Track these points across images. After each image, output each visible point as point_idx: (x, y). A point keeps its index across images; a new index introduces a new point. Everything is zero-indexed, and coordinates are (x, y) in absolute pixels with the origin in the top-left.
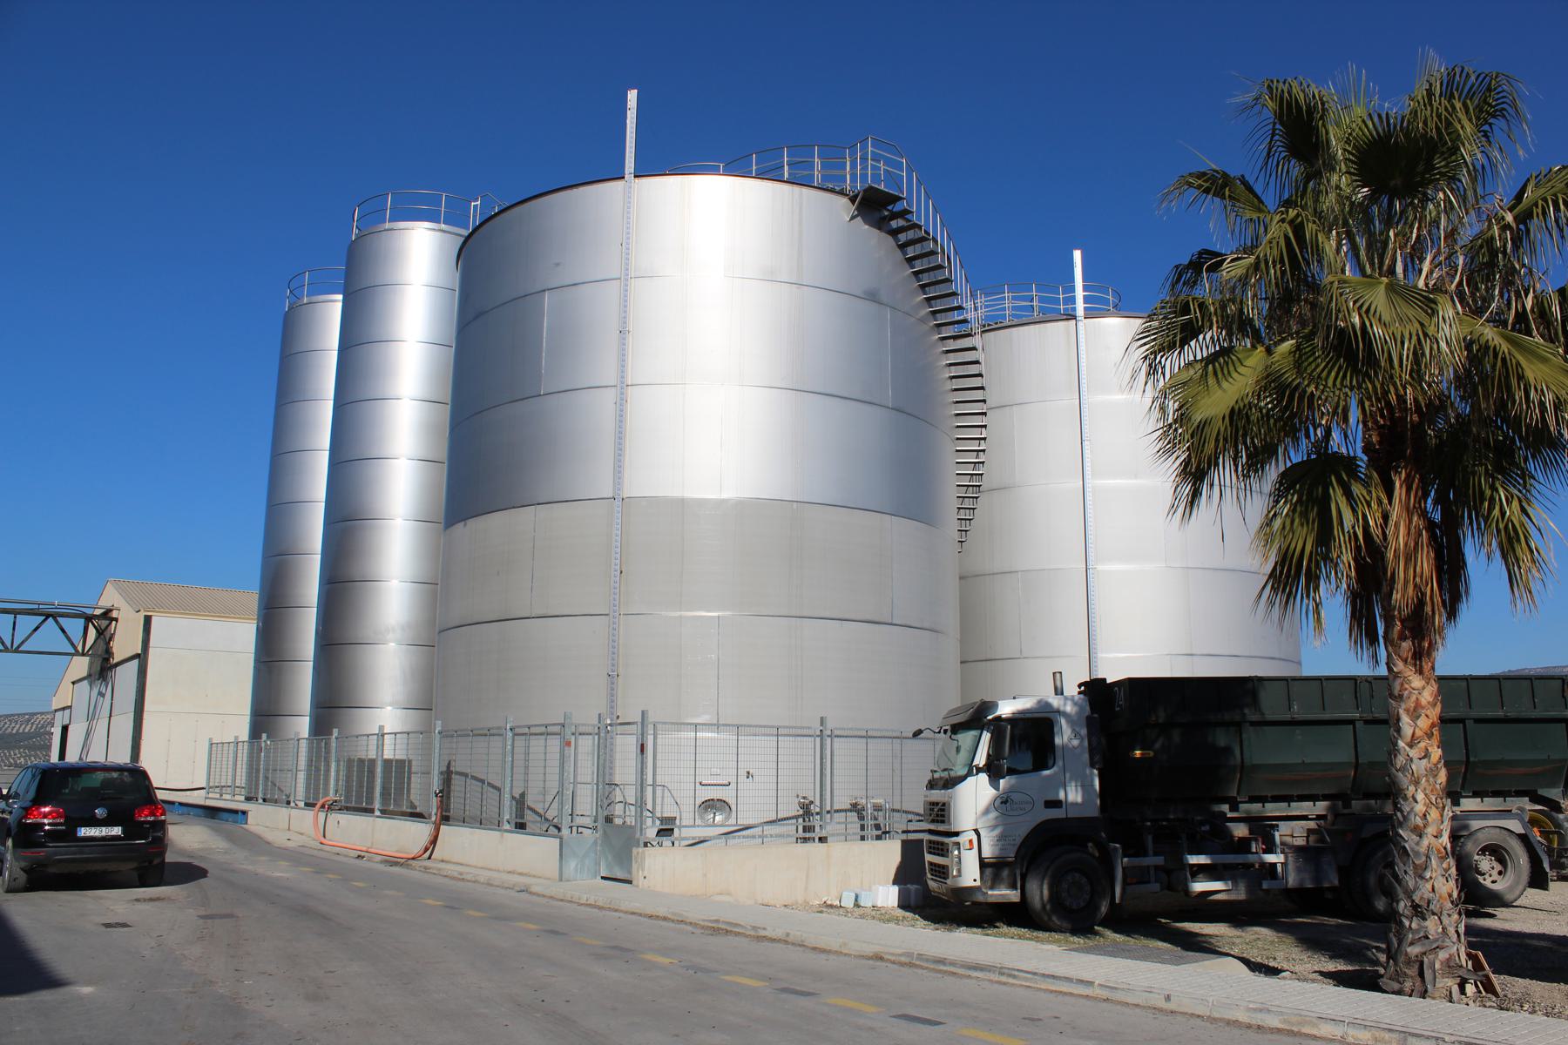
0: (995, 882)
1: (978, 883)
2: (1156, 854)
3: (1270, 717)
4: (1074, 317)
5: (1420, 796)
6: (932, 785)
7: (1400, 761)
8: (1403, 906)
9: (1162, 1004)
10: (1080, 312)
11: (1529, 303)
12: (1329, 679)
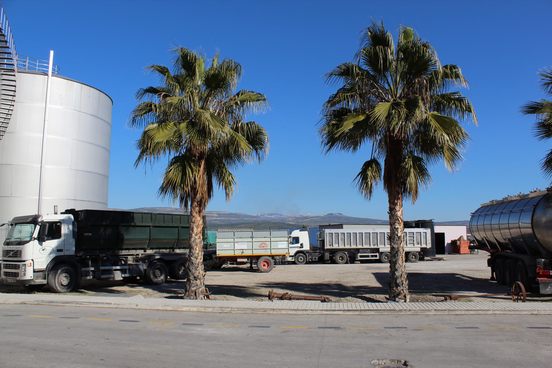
0: (37, 277)
1: (32, 278)
2: (92, 266)
3: (138, 224)
4: (47, 75)
5: (197, 249)
6: (7, 244)
7: (193, 239)
8: (192, 278)
9: (135, 307)
10: (50, 73)
11: (240, 125)
12: (157, 214)
